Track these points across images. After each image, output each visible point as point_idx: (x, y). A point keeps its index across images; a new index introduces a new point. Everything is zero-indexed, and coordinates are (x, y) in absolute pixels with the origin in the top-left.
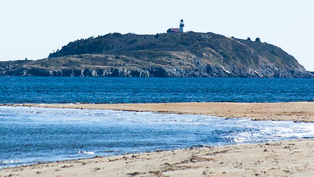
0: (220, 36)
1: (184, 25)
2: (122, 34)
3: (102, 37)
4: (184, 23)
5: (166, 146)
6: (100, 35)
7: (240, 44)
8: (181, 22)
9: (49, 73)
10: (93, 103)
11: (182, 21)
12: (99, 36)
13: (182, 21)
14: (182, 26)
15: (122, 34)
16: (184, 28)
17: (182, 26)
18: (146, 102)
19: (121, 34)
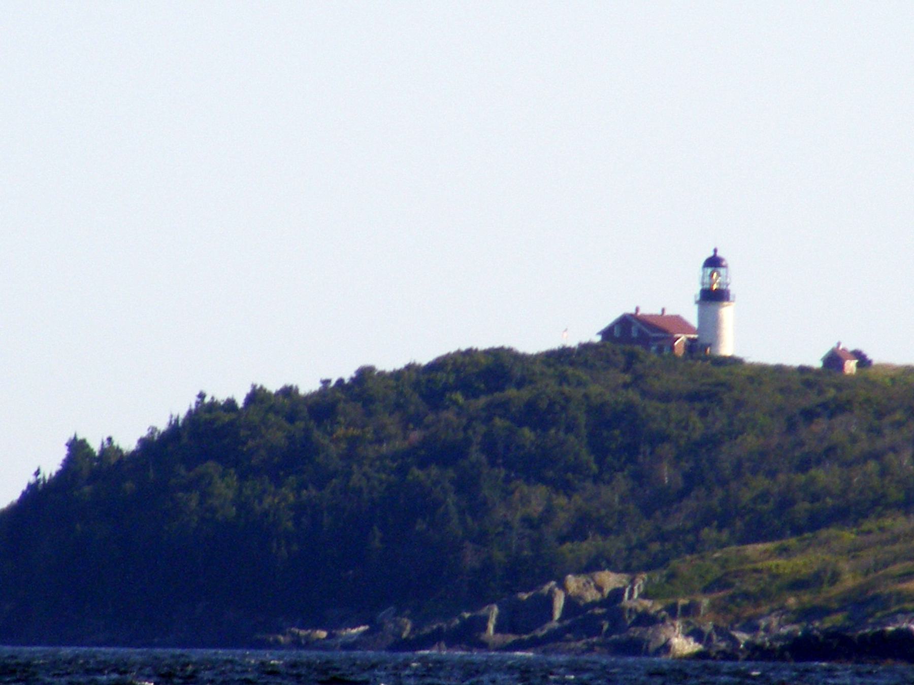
8: (709, 270)
11: (714, 262)
13: (714, 262)
16: (727, 313)
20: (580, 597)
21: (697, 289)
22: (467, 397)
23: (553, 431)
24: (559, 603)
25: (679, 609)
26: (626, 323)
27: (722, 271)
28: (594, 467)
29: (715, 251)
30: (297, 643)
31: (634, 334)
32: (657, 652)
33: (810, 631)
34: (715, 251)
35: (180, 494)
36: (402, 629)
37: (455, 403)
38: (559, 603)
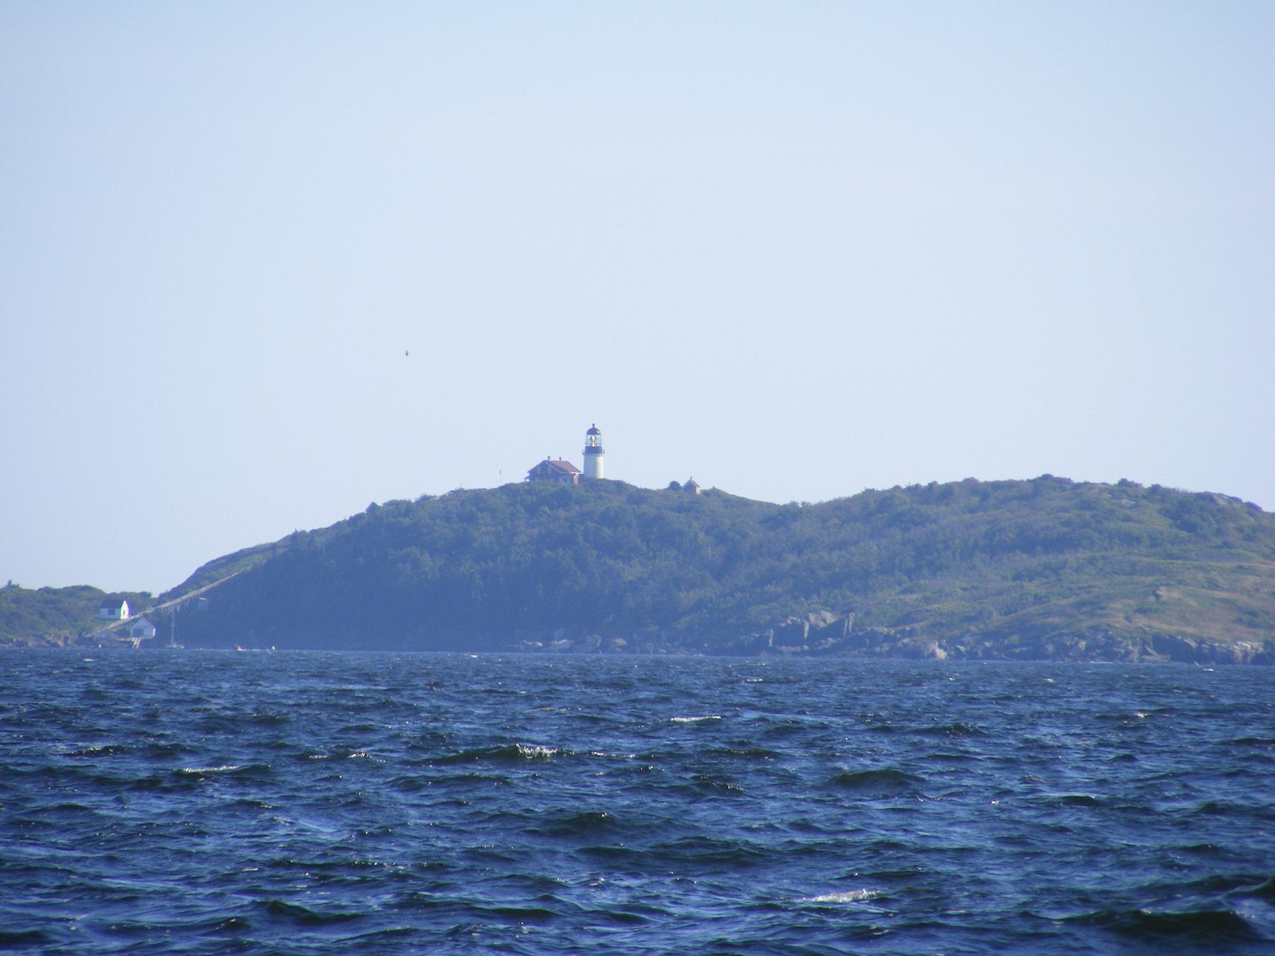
0: (200, 573)
1: (604, 447)
2: (413, 501)
3: (55, 592)
4: (605, 441)
5: (857, 846)
6: (14, 583)
7: (182, 605)
8: (589, 436)
9: (1232, 652)
10: (1164, 603)
11: (593, 431)
12: (10, 582)
13: (593, 431)
14: (592, 451)
15: (413, 501)
16: (601, 460)
17: (592, 451)
18: (659, 831)
19: (304, 532)
20: (817, 626)
21: (583, 448)
22: (551, 509)
23: (620, 529)
24: (807, 628)
25: (133, 617)
26: (545, 465)
27: (597, 436)
28: (645, 549)
29: (594, 425)
30: (528, 649)
31: (549, 472)
32: (929, 657)
33: (1256, 653)
34: (594, 425)
35: (400, 565)
36: (597, 641)
37: (545, 512)
38: (807, 628)
